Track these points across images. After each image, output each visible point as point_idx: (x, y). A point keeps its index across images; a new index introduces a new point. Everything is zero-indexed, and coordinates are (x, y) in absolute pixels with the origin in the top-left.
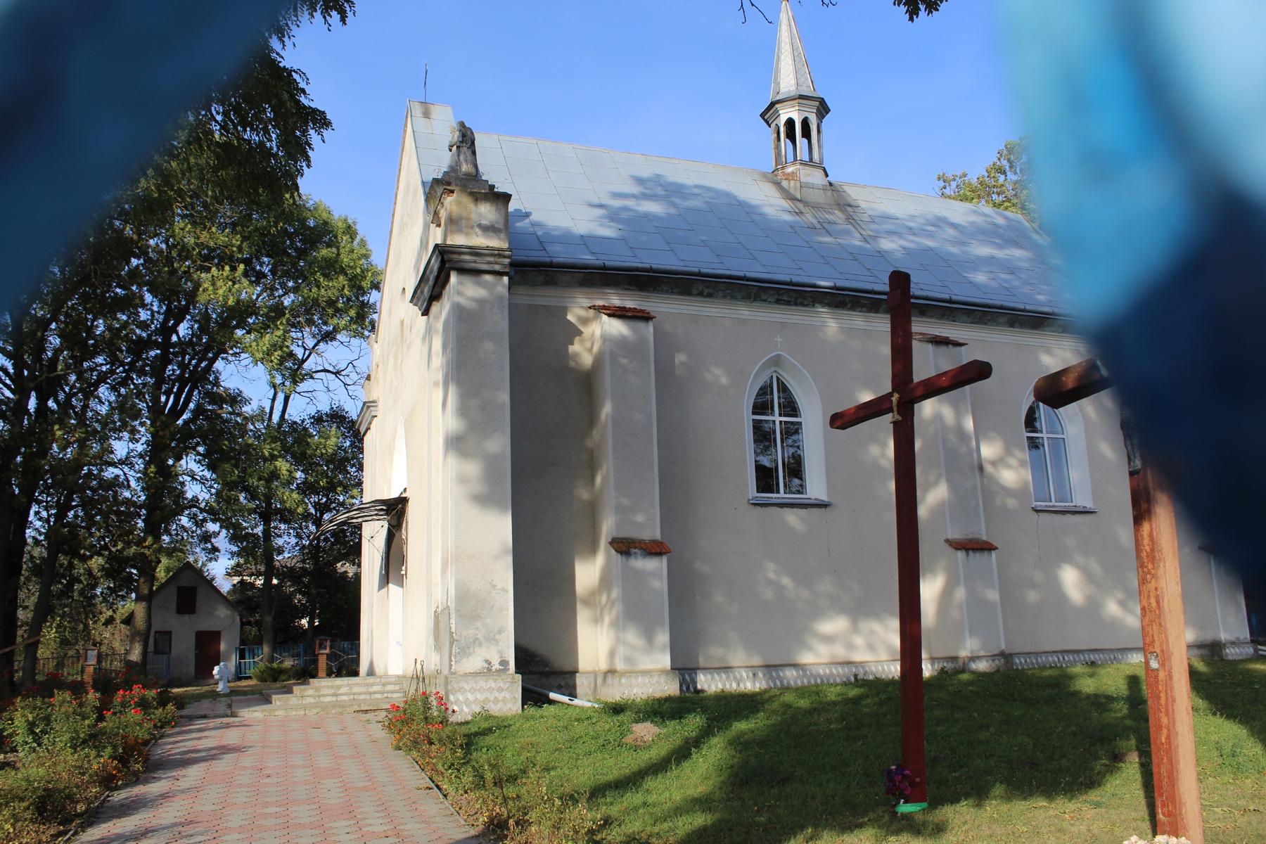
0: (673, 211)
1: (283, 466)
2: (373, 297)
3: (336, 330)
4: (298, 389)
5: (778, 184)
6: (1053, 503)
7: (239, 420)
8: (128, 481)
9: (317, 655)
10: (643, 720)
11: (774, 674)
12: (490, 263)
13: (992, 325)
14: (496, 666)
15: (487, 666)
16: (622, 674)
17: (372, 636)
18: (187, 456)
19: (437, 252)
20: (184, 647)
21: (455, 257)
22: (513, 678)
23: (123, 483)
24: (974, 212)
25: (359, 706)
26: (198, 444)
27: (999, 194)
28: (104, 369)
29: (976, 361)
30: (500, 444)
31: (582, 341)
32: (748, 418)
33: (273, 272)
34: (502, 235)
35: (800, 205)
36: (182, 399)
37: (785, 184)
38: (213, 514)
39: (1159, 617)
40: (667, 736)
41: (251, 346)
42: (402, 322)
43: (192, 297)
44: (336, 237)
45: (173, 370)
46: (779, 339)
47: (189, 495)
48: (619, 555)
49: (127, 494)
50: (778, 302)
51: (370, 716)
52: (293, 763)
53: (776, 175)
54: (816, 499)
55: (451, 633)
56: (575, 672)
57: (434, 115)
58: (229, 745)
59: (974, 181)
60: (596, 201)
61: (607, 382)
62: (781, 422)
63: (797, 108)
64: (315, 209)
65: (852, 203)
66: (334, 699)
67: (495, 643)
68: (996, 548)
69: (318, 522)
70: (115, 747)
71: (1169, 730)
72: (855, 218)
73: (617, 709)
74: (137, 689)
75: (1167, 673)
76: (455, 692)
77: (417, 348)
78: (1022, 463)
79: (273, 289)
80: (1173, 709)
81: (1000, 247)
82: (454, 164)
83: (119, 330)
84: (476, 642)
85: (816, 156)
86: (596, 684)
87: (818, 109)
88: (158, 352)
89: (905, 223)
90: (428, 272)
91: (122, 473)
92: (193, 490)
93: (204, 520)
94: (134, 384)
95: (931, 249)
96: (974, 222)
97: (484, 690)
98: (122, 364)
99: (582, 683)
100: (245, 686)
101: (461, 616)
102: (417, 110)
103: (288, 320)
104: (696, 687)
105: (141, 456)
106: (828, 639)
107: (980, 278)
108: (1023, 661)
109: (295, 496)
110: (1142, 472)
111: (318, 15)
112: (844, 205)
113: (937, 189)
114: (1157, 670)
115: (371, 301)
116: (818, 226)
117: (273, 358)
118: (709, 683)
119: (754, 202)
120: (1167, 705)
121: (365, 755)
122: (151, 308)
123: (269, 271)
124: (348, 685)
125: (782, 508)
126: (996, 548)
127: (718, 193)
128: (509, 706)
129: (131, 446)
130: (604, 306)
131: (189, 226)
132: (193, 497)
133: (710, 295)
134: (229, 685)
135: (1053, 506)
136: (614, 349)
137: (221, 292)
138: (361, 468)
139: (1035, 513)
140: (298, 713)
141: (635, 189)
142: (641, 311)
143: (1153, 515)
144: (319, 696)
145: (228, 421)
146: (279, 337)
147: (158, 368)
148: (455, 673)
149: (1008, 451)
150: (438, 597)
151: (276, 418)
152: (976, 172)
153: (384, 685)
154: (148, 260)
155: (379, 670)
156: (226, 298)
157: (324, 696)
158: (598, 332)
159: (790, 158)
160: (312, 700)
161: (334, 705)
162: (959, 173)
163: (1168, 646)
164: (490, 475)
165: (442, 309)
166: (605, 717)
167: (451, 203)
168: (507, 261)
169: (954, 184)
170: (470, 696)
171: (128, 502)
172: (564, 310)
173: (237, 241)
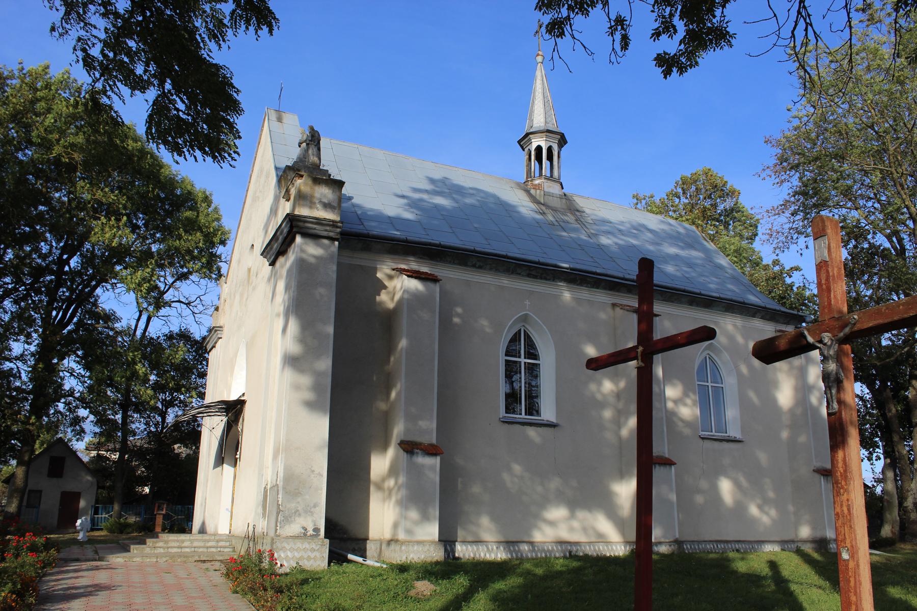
0: (455, 205)
1: (141, 368)
2: (220, 250)
3: (190, 273)
4: (159, 314)
5: (528, 192)
6: (713, 433)
7: (111, 333)
8: (20, 373)
9: (156, 515)
10: (423, 578)
11: (512, 548)
12: (326, 230)
13: (677, 303)
14: (311, 532)
15: (304, 531)
16: (403, 543)
17: (205, 503)
18: (69, 358)
19: (287, 219)
20: (51, 502)
21: (301, 224)
22: (323, 542)
23: (16, 374)
24: (663, 222)
25: (199, 556)
26: (78, 349)
27: (675, 211)
28: (10, 286)
29: (705, 327)
30: (325, 364)
32: (502, 358)
33: (146, 225)
35: (544, 208)
36: (69, 315)
37: (533, 191)
38: (83, 402)
39: (850, 521)
40: (441, 594)
41: (126, 279)
42: (249, 270)
43: (85, 237)
44: (196, 204)
45: (64, 292)
46: (527, 303)
47: (67, 387)
48: (405, 454)
49: (18, 384)
50: (529, 275)
51: (207, 565)
52: (155, 601)
53: (527, 185)
54: (547, 421)
55: (278, 505)
56: (366, 539)
57: (284, 120)
58: (101, 584)
59: (658, 202)
60: (400, 193)
61: (404, 323)
62: (525, 363)
63: (545, 139)
64: (182, 182)
65: (580, 209)
66: (179, 550)
67: (310, 514)
68: (675, 464)
69: (163, 415)
70: (14, 584)
71: (857, 606)
72: (582, 220)
73: (403, 569)
74: (28, 536)
75: (855, 563)
77: (262, 287)
79: (145, 238)
80: (860, 591)
81: (682, 248)
82: (302, 156)
83: (25, 258)
84: (297, 513)
85: (556, 174)
86: (381, 549)
87: (559, 141)
88: (53, 277)
89: (616, 226)
90: (278, 233)
91: (16, 367)
92: (70, 383)
93: (77, 407)
94: (32, 300)
95: (634, 246)
96: (663, 230)
97: (315, 550)
98: (24, 284)
99: (371, 548)
100: (98, 536)
101: (286, 492)
102: (273, 115)
103: (156, 261)
104: (455, 555)
105: (33, 355)
106: (552, 523)
108: (689, 547)
109: (149, 392)
110: (838, 414)
111: (252, 29)
112: (573, 209)
113: (632, 205)
114: (848, 560)
115: (218, 253)
116: (556, 223)
117: (142, 288)
118: (463, 551)
119: (515, 203)
120: (855, 587)
121: (210, 597)
122: (50, 245)
123: (143, 224)
124: (190, 540)
125: (523, 425)
126: (675, 464)
127: (488, 195)
128: (318, 563)
129: (26, 346)
130: (405, 269)
131: (88, 185)
132: (70, 389)
133: (480, 267)
134: (87, 534)
135: (713, 436)
136: (412, 301)
137: (107, 236)
138: (203, 375)
139: (701, 440)
140: (152, 560)
141: (429, 187)
142: (430, 275)
143: (846, 446)
144: (168, 548)
145: (101, 333)
146: (149, 273)
147: (52, 293)
148: (279, 536)
149: (686, 394)
150: (269, 477)
151: (139, 333)
152: (660, 195)
153: (218, 541)
154: (52, 208)
155: (210, 528)
156: (111, 241)
157: (172, 547)
158: (399, 286)
159: (537, 174)
160: (162, 550)
161: (180, 555)
163: (856, 543)
164: (316, 388)
165: (286, 263)
166: (393, 575)
167: (301, 183)
168: (339, 230)
169: (644, 202)
170: (289, 554)
171: (18, 389)
172: (375, 270)
173: (123, 200)
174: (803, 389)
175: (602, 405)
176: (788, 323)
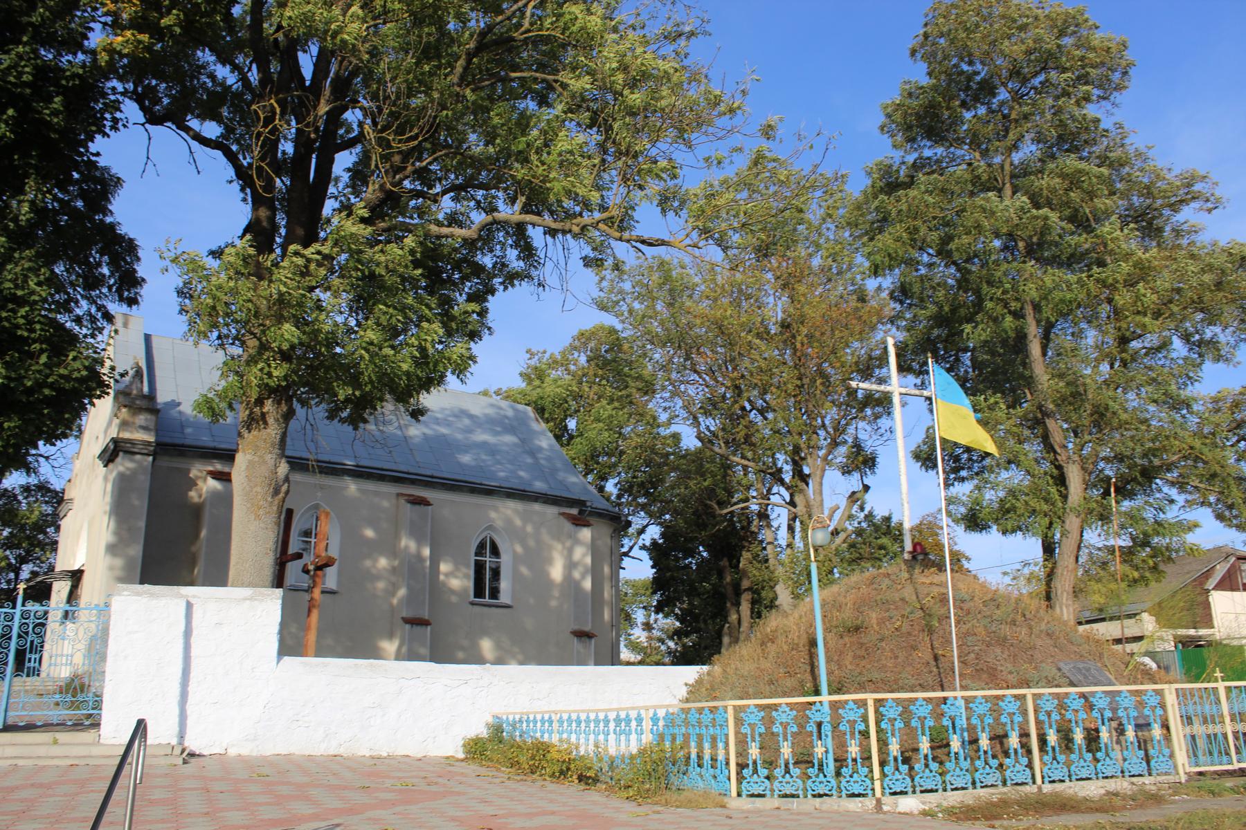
30: (136, 550)
31: (197, 490)
34: (153, 433)
76: (95, 681)
78: (466, 576)
81: (496, 433)
95: (444, 435)
107: (466, 459)
138: (58, 528)
149: (457, 569)
162: (541, 350)
169: (536, 357)
172: (188, 471)
174: (570, 565)
175: (378, 577)
176: (571, 507)
